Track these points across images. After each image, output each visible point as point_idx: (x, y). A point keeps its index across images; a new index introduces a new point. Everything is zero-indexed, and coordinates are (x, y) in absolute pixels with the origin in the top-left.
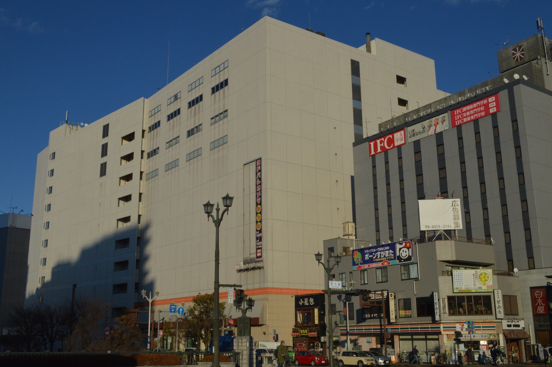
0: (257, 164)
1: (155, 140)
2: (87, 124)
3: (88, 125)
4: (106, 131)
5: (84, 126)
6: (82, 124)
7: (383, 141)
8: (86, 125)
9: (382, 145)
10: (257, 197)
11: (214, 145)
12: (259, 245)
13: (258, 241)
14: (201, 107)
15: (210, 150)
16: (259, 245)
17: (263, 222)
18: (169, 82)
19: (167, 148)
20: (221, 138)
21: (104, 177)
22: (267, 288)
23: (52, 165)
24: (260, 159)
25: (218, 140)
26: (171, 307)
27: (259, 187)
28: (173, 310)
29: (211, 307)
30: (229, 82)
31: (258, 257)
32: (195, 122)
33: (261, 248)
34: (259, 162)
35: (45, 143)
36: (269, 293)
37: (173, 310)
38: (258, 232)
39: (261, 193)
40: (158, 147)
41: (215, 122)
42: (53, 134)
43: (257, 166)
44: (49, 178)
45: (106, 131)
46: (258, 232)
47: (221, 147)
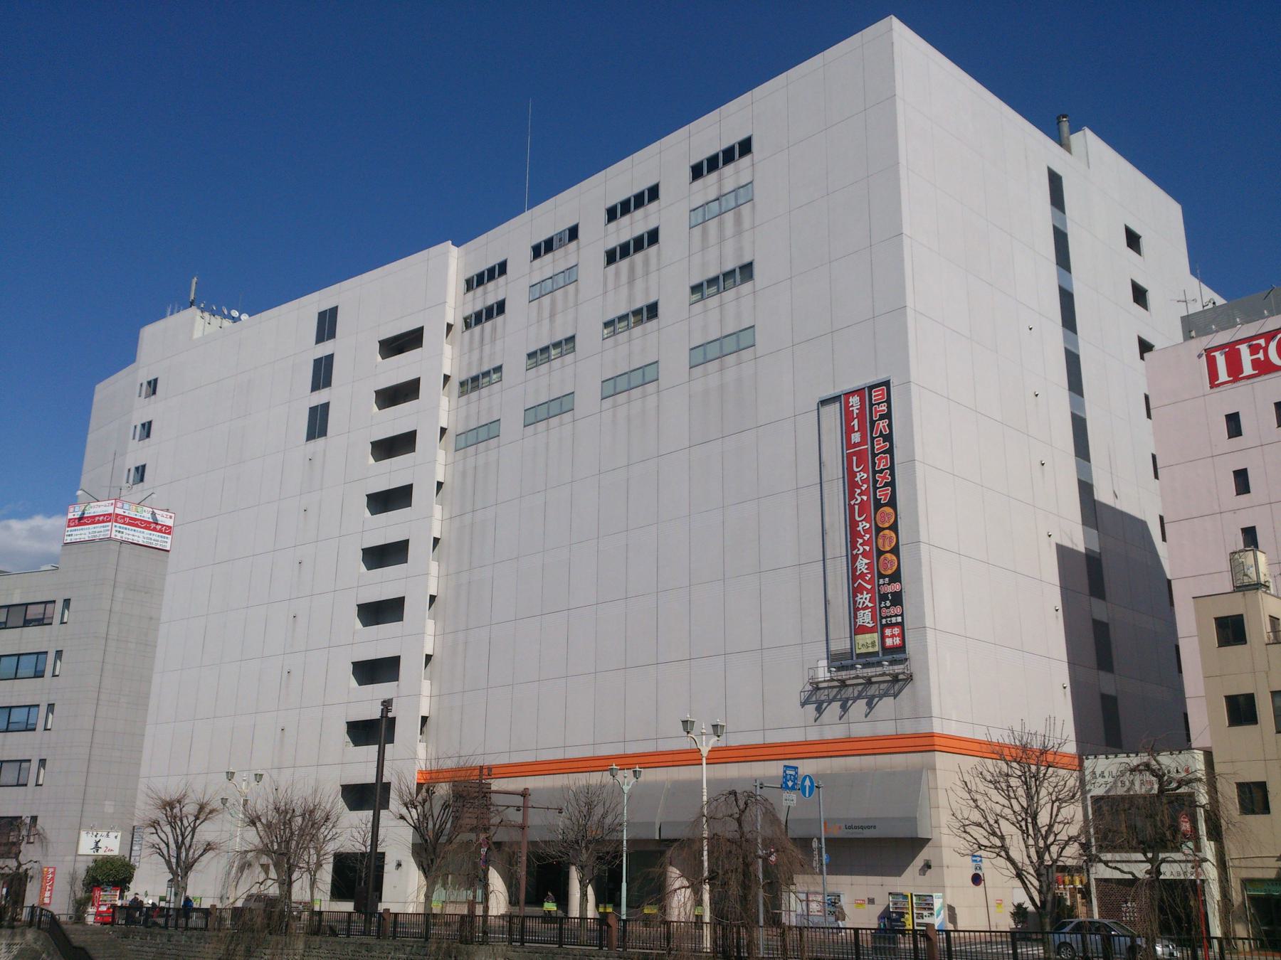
0: (874, 399)
1: (487, 348)
2: (247, 316)
3: (250, 316)
4: (327, 325)
5: (239, 319)
6: (235, 313)
7: (1264, 345)
8: (244, 317)
9: (1261, 355)
10: (878, 486)
11: (548, 409)
12: (891, 617)
13: (888, 603)
14: (499, 330)
15: (525, 426)
16: (891, 617)
17: (903, 551)
18: (534, 203)
19: (528, 367)
20: (610, 379)
21: (320, 442)
22: (932, 735)
23: (144, 410)
24: (887, 384)
25: (612, 380)
26: (787, 772)
27: (882, 458)
28: (790, 784)
29: (12, 834)
30: (662, 236)
31: (886, 650)
32: (631, 298)
33: (901, 625)
34: (882, 394)
35: (127, 355)
36: (937, 748)
37: (790, 784)
38: (887, 579)
39: (892, 474)
40: (497, 364)
41: (614, 333)
42: (151, 335)
43: (874, 402)
44: (134, 444)
45: (327, 325)
46: (887, 579)
47: (482, 446)
